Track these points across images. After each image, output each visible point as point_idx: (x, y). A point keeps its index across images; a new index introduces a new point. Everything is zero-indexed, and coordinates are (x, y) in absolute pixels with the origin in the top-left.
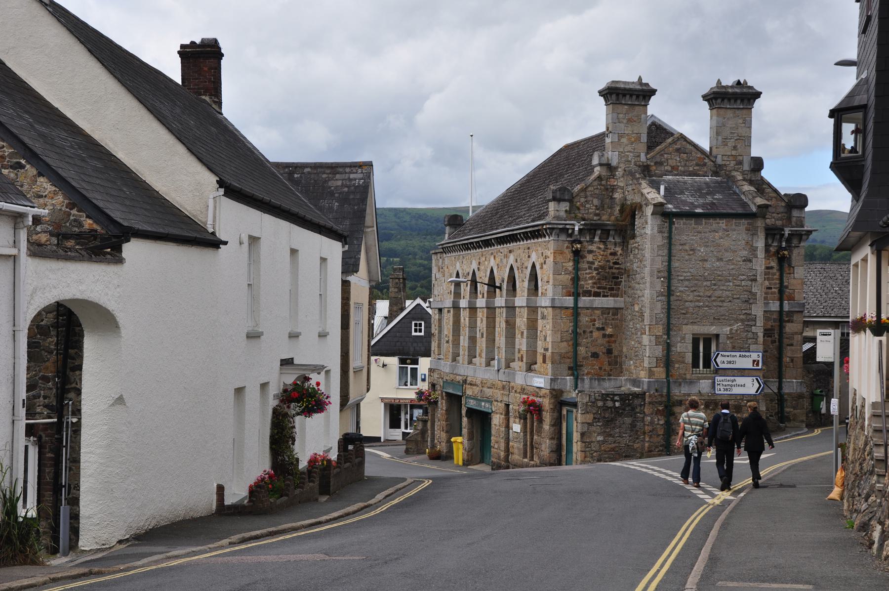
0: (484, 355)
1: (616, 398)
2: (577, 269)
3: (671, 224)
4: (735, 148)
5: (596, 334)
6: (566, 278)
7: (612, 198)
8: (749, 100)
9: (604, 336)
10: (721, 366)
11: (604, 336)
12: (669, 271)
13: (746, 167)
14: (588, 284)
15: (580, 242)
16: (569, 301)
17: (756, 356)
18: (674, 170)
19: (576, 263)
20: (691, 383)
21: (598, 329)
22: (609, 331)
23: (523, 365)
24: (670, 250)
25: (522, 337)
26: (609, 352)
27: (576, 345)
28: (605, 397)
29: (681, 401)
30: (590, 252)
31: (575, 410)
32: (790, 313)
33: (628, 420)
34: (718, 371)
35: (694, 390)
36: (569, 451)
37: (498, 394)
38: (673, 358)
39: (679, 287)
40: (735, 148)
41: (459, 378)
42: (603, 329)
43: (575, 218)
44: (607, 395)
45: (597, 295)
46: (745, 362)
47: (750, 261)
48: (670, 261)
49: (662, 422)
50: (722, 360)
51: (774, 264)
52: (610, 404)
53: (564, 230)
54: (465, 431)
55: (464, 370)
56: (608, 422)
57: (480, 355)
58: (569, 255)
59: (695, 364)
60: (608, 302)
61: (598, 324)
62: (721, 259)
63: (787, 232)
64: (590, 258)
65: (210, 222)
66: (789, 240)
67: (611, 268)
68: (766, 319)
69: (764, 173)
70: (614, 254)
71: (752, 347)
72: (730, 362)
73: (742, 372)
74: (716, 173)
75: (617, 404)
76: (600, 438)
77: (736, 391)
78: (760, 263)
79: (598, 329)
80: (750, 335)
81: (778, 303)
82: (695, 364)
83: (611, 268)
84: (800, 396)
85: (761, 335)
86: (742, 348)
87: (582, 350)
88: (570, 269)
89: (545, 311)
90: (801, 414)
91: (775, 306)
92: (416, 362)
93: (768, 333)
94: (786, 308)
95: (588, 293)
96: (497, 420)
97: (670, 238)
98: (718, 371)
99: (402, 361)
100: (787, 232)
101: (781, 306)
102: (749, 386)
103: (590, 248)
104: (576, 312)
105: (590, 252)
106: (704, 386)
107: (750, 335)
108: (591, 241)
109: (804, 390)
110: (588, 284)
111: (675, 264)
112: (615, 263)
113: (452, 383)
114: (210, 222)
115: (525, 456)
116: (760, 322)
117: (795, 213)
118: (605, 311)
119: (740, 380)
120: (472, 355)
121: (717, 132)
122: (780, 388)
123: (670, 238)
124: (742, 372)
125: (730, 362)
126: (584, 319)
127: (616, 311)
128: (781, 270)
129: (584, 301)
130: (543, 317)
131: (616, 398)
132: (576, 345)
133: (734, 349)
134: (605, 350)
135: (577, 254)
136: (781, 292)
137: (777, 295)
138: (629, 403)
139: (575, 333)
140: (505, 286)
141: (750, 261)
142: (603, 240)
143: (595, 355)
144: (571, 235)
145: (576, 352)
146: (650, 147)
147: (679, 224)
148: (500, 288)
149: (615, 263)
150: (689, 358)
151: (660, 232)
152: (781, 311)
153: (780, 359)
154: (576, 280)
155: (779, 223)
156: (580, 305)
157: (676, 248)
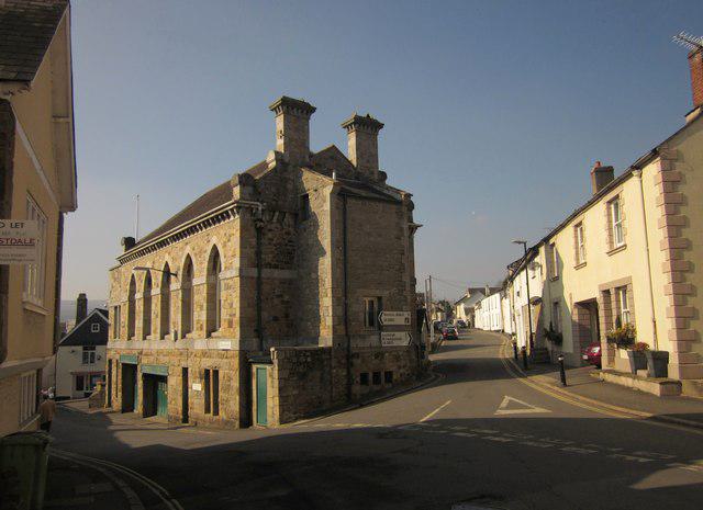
0: (159, 331)
1: (308, 354)
2: (259, 244)
4: (368, 161)
5: (276, 301)
6: (251, 252)
7: (285, 187)
9: (283, 302)
14: (268, 258)
15: (261, 221)
16: (254, 272)
17: (407, 314)
19: (259, 239)
20: (363, 337)
21: (278, 296)
22: (286, 298)
23: (204, 333)
24: (345, 223)
25: (201, 309)
26: (287, 316)
27: (259, 310)
28: (298, 354)
29: (358, 354)
30: (270, 230)
31: (268, 367)
33: (318, 374)
35: (367, 344)
37: (175, 360)
41: (136, 352)
42: (281, 296)
45: (276, 267)
48: (345, 234)
49: (344, 373)
52: (302, 359)
54: (302, 426)
55: (138, 343)
56: (303, 376)
57: (155, 332)
61: (277, 292)
64: (270, 235)
69: (388, 182)
70: (288, 233)
73: (398, 328)
74: (357, 178)
76: (295, 392)
79: (278, 296)
87: (265, 315)
88: (254, 243)
89: (230, 282)
92: (94, 349)
95: (270, 266)
96: (174, 382)
99: (85, 349)
105: (270, 230)
106: (374, 340)
111: (349, 236)
112: (290, 241)
113: (128, 356)
115: (207, 410)
118: (283, 282)
119: (398, 334)
120: (147, 333)
124: (398, 328)
126: (266, 288)
127: (291, 282)
129: (266, 272)
130: (228, 287)
131: (308, 354)
132: (259, 310)
133: (392, 309)
135: (259, 230)
139: (259, 298)
140: (180, 273)
143: (276, 319)
145: (259, 315)
147: (351, 202)
148: (176, 275)
149: (290, 241)
151: (337, 208)
154: (258, 253)
156: (263, 275)
157: (349, 222)
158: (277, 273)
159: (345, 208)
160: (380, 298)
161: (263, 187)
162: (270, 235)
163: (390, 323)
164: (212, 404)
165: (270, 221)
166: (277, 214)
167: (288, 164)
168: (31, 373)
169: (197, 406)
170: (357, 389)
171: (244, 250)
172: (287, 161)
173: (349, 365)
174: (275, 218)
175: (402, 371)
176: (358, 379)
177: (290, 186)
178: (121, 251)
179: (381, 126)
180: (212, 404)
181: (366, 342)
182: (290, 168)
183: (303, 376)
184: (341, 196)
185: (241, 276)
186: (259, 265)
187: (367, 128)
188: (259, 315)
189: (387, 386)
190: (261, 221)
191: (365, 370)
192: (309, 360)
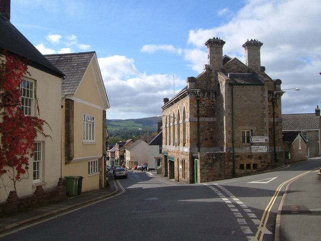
2: (198, 107)
3: (232, 88)
4: (255, 63)
5: (206, 131)
6: (195, 111)
8: (259, 46)
9: (210, 132)
10: (254, 142)
11: (210, 132)
12: (232, 106)
13: (259, 70)
14: (203, 113)
16: (196, 119)
17: (267, 138)
18: (233, 70)
22: (211, 130)
30: (204, 101)
32: (277, 123)
34: (252, 144)
36: (197, 180)
38: (235, 139)
39: (237, 112)
40: (255, 63)
43: (197, 88)
44: (210, 154)
45: (206, 116)
46: (262, 140)
47: (263, 102)
50: (254, 139)
51: (271, 104)
53: (193, 92)
58: (196, 102)
59: (244, 142)
60: (211, 119)
61: (207, 127)
62: (252, 101)
63: (275, 92)
64: (203, 103)
65: (119, 184)
66: (276, 96)
67: (211, 106)
68: (269, 125)
71: (265, 134)
72: (257, 140)
73: (261, 144)
74: (248, 72)
75: (214, 157)
77: (260, 151)
78: (267, 103)
80: (264, 130)
81: (273, 119)
82: (244, 142)
83: (211, 106)
84: (282, 153)
85: (268, 130)
86: (261, 135)
87: (201, 138)
88: (196, 107)
90: (282, 159)
91: (272, 120)
93: (270, 130)
94: (276, 121)
95: (203, 116)
97: (232, 93)
98: (252, 144)
100: (275, 92)
101: (274, 120)
102: (264, 149)
103: (203, 99)
104: (198, 123)
105: (204, 101)
107: (264, 130)
108: (203, 97)
109: (283, 150)
110: (203, 113)
111: (235, 103)
114: (119, 184)
116: (267, 125)
117: (277, 86)
118: (210, 123)
121: (250, 60)
122: (275, 150)
123: (232, 93)
124: (261, 144)
125: (257, 140)
126: (201, 126)
127: (214, 123)
128: (274, 107)
129: (201, 119)
134: (210, 137)
135: (198, 102)
136: (274, 114)
137: (272, 116)
138: (219, 156)
141: (263, 102)
142: (208, 96)
143: (206, 139)
144: (196, 94)
145: (198, 138)
146: (224, 64)
147: (235, 87)
150: (241, 139)
152: (274, 122)
153: (274, 139)
154: (198, 111)
155: (272, 90)
158: (207, 119)
159: (232, 91)
160: (252, 130)
161: (200, 82)
162: (203, 103)
163: (256, 142)
164: (184, 176)
165: (203, 97)
166: (206, 93)
167: (212, 70)
168: (95, 160)
169: (181, 177)
170: (237, 171)
171: (192, 110)
172: (211, 68)
173: (234, 161)
174: (206, 95)
175: (263, 164)
176: (239, 167)
177: (213, 80)
178: (163, 104)
179: (261, 44)
180: (184, 176)
181: (242, 151)
182: (213, 71)
183: (211, 165)
184: (231, 84)
185: (190, 121)
186: (198, 116)
187: (253, 46)
188: (198, 138)
189: (254, 170)
190: (199, 97)
191: (242, 163)
192: (214, 157)
